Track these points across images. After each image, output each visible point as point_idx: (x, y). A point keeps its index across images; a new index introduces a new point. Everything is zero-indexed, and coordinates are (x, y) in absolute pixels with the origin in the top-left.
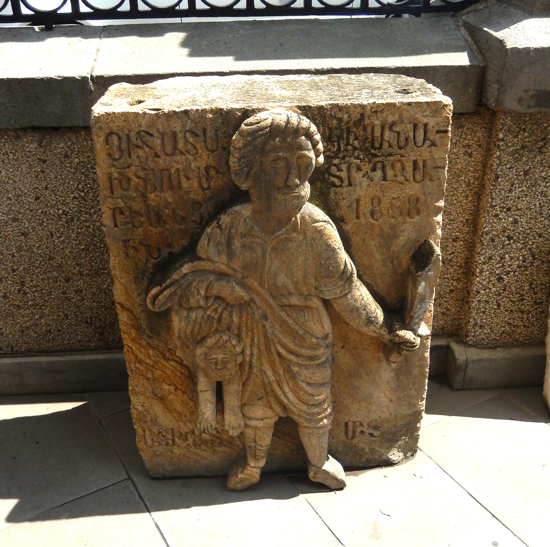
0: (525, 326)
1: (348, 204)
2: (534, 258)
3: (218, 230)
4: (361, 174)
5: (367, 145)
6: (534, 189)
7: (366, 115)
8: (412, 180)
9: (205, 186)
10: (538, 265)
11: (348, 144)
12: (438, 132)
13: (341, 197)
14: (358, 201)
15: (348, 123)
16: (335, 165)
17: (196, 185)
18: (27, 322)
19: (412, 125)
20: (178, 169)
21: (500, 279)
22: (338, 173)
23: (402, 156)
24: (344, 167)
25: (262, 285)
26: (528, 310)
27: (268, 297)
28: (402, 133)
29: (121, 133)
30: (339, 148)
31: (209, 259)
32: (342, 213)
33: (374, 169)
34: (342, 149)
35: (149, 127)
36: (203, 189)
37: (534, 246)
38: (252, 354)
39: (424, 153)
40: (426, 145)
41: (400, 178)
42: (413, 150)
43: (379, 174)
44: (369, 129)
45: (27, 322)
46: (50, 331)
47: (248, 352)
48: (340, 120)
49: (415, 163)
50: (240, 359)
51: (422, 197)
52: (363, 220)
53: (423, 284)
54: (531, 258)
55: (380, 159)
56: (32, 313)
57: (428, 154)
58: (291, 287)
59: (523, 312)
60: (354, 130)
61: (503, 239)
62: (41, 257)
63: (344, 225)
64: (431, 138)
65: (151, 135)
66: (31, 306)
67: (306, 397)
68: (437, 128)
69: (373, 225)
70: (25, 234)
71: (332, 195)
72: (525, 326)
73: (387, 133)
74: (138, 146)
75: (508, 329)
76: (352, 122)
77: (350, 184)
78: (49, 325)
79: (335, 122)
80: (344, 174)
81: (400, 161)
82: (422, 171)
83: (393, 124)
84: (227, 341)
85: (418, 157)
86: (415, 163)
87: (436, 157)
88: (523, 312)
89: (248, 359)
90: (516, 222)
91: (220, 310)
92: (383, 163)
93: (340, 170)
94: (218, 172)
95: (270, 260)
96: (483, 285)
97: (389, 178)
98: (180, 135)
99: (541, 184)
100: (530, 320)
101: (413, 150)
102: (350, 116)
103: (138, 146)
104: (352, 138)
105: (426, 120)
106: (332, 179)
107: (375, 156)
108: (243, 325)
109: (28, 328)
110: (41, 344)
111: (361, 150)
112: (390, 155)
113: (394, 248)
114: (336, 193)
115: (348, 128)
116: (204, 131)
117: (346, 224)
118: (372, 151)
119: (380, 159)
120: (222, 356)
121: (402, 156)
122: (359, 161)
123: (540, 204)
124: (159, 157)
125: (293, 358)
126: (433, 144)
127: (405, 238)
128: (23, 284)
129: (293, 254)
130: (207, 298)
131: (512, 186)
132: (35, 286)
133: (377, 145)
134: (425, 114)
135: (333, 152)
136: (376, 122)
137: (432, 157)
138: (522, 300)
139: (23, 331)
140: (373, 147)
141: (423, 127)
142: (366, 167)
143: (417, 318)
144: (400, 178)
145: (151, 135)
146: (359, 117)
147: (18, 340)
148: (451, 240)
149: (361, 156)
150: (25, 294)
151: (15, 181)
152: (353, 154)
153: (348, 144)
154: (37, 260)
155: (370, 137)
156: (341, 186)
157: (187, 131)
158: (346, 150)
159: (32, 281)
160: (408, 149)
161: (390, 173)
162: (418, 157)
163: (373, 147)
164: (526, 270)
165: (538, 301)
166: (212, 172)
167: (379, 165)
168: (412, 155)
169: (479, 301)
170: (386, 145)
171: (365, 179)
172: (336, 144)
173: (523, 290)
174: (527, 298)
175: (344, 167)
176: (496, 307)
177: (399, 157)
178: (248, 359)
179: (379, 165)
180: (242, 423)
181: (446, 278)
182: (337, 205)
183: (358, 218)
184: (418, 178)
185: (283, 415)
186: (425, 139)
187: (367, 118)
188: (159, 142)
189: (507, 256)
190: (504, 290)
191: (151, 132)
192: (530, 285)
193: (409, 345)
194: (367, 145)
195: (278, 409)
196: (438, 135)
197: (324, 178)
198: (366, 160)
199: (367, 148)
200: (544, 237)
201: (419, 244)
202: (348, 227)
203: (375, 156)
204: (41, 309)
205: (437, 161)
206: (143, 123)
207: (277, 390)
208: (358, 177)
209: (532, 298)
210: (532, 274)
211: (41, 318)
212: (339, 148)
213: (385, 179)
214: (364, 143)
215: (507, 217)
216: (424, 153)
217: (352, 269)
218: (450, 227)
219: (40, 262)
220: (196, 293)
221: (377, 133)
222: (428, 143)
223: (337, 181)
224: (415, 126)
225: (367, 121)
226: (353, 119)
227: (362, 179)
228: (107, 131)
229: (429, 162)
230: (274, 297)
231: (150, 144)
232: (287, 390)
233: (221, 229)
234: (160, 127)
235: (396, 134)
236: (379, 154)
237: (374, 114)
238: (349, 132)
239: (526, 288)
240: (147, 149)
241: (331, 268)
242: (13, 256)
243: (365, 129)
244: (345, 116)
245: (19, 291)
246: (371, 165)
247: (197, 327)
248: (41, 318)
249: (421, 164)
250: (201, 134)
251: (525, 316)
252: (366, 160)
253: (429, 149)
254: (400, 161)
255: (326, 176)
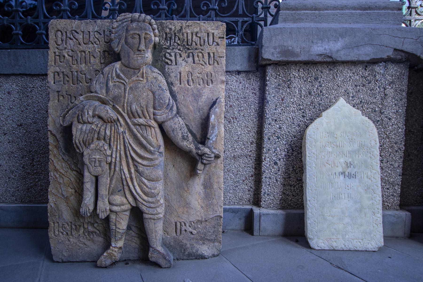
0: (293, 196)
1: (175, 75)
2: (293, 151)
3: (102, 75)
4: (182, 58)
5: (184, 43)
6: (288, 108)
7: (183, 28)
8: (208, 64)
9: (102, 61)
10: (296, 155)
11: (175, 42)
12: (220, 38)
13: (171, 71)
14: (180, 74)
15: (174, 31)
16: (168, 53)
17: (97, 61)
18: (31, 183)
19: (207, 34)
20: (89, 52)
21: (276, 163)
22: (170, 58)
23: (202, 50)
24: (173, 54)
25: (124, 110)
26: (294, 184)
27: (127, 118)
28: (201, 37)
29: (62, 31)
30: (170, 44)
31: (96, 92)
32: (172, 80)
33: (189, 57)
34: (172, 45)
35: (77, 28)
36: (101, 63)
37: (292, 143)
38: (116, 157)
39: (213, 48)
40: (214, 45)
41: (202, 62)
42: (207, 47)
43: (191, 59)
44: (185, 35)
45: (31, 183)
46: (42, 190)
47: (114, 156)
48: (171, 29)
49: (209, 54)
50: (109, 159)
51: (213, 74)
52: (183, 85)
53: (213, 116)
54: (291, 150)
55: (191, 51)
56: (35, 178)
57: (215, 49)
58: (140, 112)
59: (291, 186)
60: (177, 35)
61: (275, 138)
62: (44, 144)
63: (173, 87)
64: (216, 41)
65: (78, 33)
66: (35, 173)
67: (147, 190)
68: (218, 36)
69: (188, 88)
70: (38, 131)
71: (166, 69)
72: (293, 196)
73: (194, 37)
74: (71, 39)
75: (284, 197)
76: (176, 30)
77: (176, 64)
78: (42, 186)
79: (168, 30)
80: (173, 58)
81: (201, 52)
82: (213, 59)
83: (197, 33)
84: (102, 146)
85: (210, 51)
86: (209, 54)
87: (219, 51)
88: (291, 186)
89: (113, 160)
90: (280, 128)
91: (99, 126)
92: (192, 53)
93: (171, 56)
94: (109, 54)
95: (129, 94)
96: (267, 167)
97: (196, 62)
98: (91, 33)
99: (292, 106)
100: (295, 191)
101: (207, 47)
102: (175, 28)
103: (71, 39)
104: (177, 39)
105: (213, 31)
106: (167, 60)
107: (189, 49)
108: (112, 136)
109: (31, 187)
110: (36, 198)
111: (182, 46)
112: (196, 49)
113: (200, 103)
114: (168, 68)
115: (175, 34)
116: (104, 31)
117: (174, 87)
118: (187, 47)
119: (191, 51)
120: (98, 157)
121: (202, 50)
122: (180, 52)
123: (292, 117)
124: (80, 45)
125: (139, 160)
126: (218, 44)
127: (206, 97)
128: (33, 159)
129: (140, 91)
130: (93, 117)
131: (276, 106)
132: (38, 162)
133: (190, 44)
134: (212, 28)
135: (167, 46)
136: (189, 31)
137: (217, 51)
138: (290, 177)
139: (29, 189)
140: (188, 45)
141: (212, 35)
142: (184, 55)
143: (211, 140)
144: (202, 62)
145: (78, 33)
146: (180, 28)
147: (25, 195)
148: (250, 143)
149: (181, 49)
150: (33, 166)
151: (39, 102)
152: (177, 47)
153: (175, 42)
154: (42, 146)
155: (186, 39)
156: (171, 65)
157: (95, 31)
158: (174, 45)
159: (38, 158)
160: (205, 46)
161: (196, 59)
162: (210, 51)
163: (188, 45)
164: (290, 157)
165: (299, 179)
166: (106, 54)
167: (191, 54)
168: (207, 49)
169: (266, 177)
170: (194, 43)
171: (183, 62)
172: (169, 42)
173: (289, 171)
174: (292, 176)
175: (173, 54)
176: (275, 181)
177: (201, 50)
178: (113, 160)
179: (191, 54)
180: (108, 208)
181: (249, 167)
182: (169, 75)
183: (180, 84)
184: (212, 62)
185: (134, 205)
186: (213, 41)
187: (184, 29)
188: (81, 37)
189: (278, 149)
190: (279, 170)
191: (77, 31)
192: (293, 168)
193: (207, 155)
194: (184, 43)
195: (131, 199)
196: (219, 40)
197: (162, 60)
198: (184, 51)
199: (184, 45)
200: (297, 137)
201: (213, 101)
202: (175, 89)
203: (189, 49)
204: (39, 175)
205: (220, 53)
206: (74, 26)
207: (130, 184)
208: (180, 60)
209: (295, 177)
210: (293, 160)
211: (39, 181)
212: (170, 44)
213: (194, 63)
214: (183, 42)
215: (275, 125)
216: (213, 48)
217: (173, 103)
218: (249, 135)
219: (43, 147)
220: (86, 113)
221: (190, 37)
222: (215, 43)
223: (169, 62)
224: (208, 34)
225: (184, 31)
226: (177, 29)
227: (182, 62)
228: (56, 29)
229: (215, 54)
230: (130, 118)
231: (76, 37)
232: (136, 184)
233: (103, 74)
234: (82, 29)
235: (199, 38)
236: (190, 48)
237: (187, 27)
238: (175, 35)
239: (291, 170)
240: (74, 40)
241: (161, 101)
242: (31, 143)
243: (183, 34)
244: (173, 27)
245: (31, 163)
246: (187, 54)
247: (86, 136)
248: (39, 181)
249: (212, 55)
250: (102, 33)
251: (292, 188)
252: (184, 51)
253: (215, 47)
254: (201, 52)
255: (164, 58)
